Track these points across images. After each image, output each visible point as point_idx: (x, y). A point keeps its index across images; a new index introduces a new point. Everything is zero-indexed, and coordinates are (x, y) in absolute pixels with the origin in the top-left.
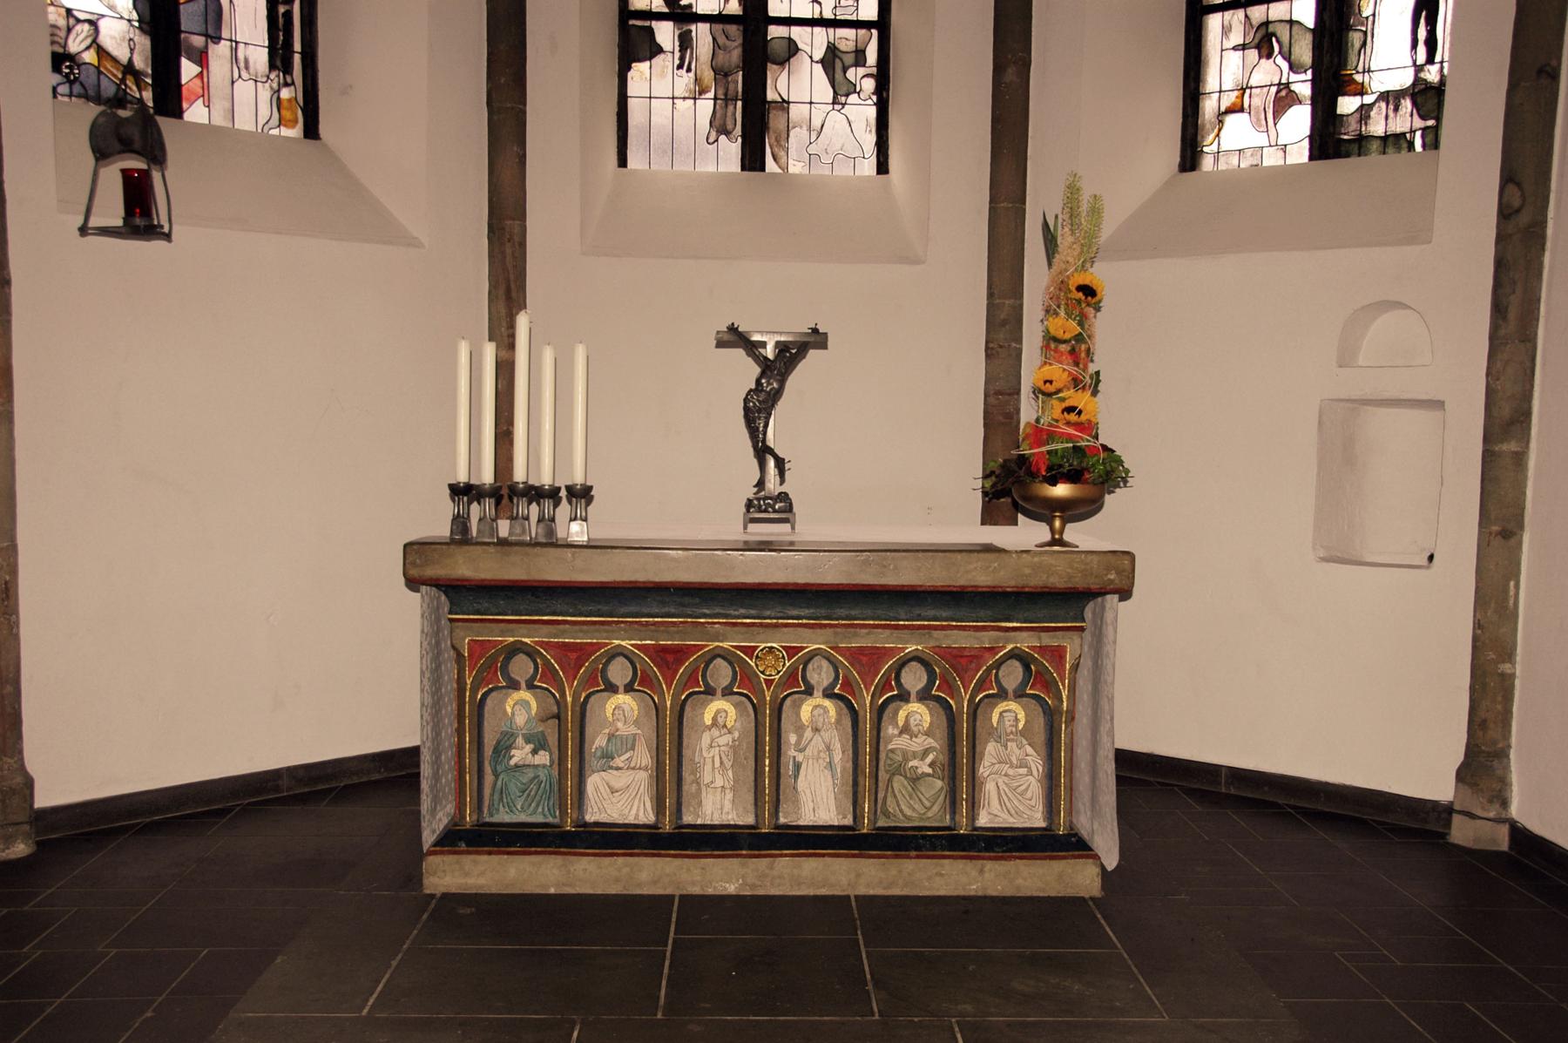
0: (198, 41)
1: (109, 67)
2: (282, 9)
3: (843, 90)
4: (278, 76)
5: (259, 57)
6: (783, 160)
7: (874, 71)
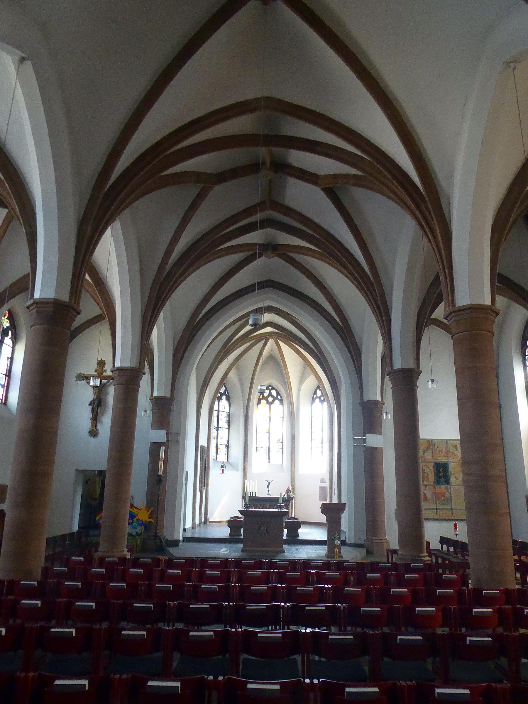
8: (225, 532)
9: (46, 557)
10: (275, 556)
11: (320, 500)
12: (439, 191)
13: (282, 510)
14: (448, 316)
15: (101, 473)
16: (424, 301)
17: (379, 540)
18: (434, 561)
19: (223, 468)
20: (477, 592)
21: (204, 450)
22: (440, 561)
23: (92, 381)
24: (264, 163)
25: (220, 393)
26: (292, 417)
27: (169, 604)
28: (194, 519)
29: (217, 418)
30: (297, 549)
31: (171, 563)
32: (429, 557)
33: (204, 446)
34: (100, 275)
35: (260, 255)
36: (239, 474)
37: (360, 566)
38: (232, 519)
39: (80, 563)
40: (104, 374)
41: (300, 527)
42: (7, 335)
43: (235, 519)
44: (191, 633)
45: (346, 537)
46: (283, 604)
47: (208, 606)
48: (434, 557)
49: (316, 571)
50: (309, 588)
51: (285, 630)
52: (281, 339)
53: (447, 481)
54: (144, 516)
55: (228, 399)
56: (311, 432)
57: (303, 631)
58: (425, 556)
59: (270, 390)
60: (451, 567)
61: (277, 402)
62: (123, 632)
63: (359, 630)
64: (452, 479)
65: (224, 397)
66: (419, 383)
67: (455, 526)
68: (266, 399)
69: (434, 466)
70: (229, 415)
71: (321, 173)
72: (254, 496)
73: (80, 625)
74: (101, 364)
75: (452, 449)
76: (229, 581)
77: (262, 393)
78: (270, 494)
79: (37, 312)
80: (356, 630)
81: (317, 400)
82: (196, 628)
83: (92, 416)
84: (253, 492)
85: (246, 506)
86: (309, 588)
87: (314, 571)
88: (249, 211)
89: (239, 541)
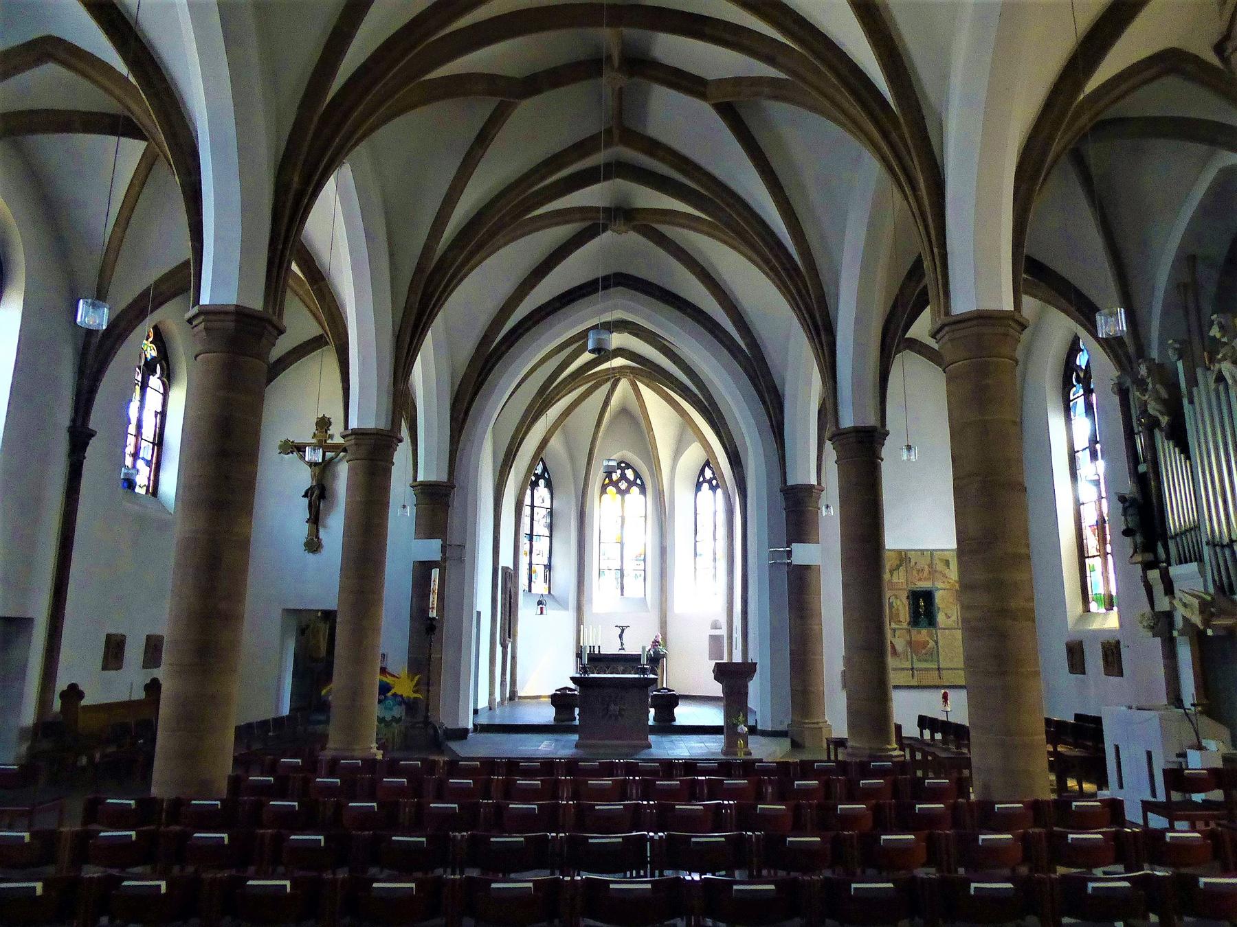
8: (547, 714)
9: (236, 759)
10: (637, 754)
11: (711, 658)
12: (923, 106)
13: (646, 676)
14: (938, 331)
15: (329, 616)
16: (895, 306)
17: (813, 723)
18: (908, 757)
19: (541, 606)
20: (985, 806)
21: (508, 574)
22: (919, 756)
23: (309, 455)
24: (609, 57)
25: (536, 475)
26: (661, 515)
27: (455, 836)
28: (491, 693)
29: (529, 518)
30: (672, 741)
31: (454, 767)
32: (901, 750)
33: (508, 568)
34: (317, 264)
35: (605, 229)
36: (569, 616)
37: (783, 767)
38: (558, 692)
39: (295, 768)
40: (329, 441)
41: (677, 704)
42: (154, 372)
43: (563, 691)
44: (493, 885)
45: (756, 720)
46: (651, 834)
47: (522, 839)
48: (908, 751)
49: (707, 777)
50: (697, 806)
51: (654, 877)
52: (644, 379)
53: (931, 622)
54: (404, 687)
55: (549, 485)
56: (696, 542)
57: (688, 878)
58: (895, 749)
59: (623, 470)
60: (940, 767)
61: (635, 490)
62: (375, 885)
63: (782, 873)
64: (941, 618)
65: (542, 482)
66: (884, 452)
67: (945, 697)
68: (615, 484)
69: (908, 598)
70: (551, 513)
71: (711, 75)
72: (596, 652)
73: (298, 874)
74: (324, 423)
75: (940, 566)
76: (556, 796)
77: (609, 474)
78: (624, 649)
79: (207, 329)
80: (776, 874)
81: (706, 486)
82: (501, 875)
83: (310, 517)
84: (594, 647)
85: (584, 670)
86: (697, 806)
87: (704, 778)
88: (582, 148)
89: (571, 730)
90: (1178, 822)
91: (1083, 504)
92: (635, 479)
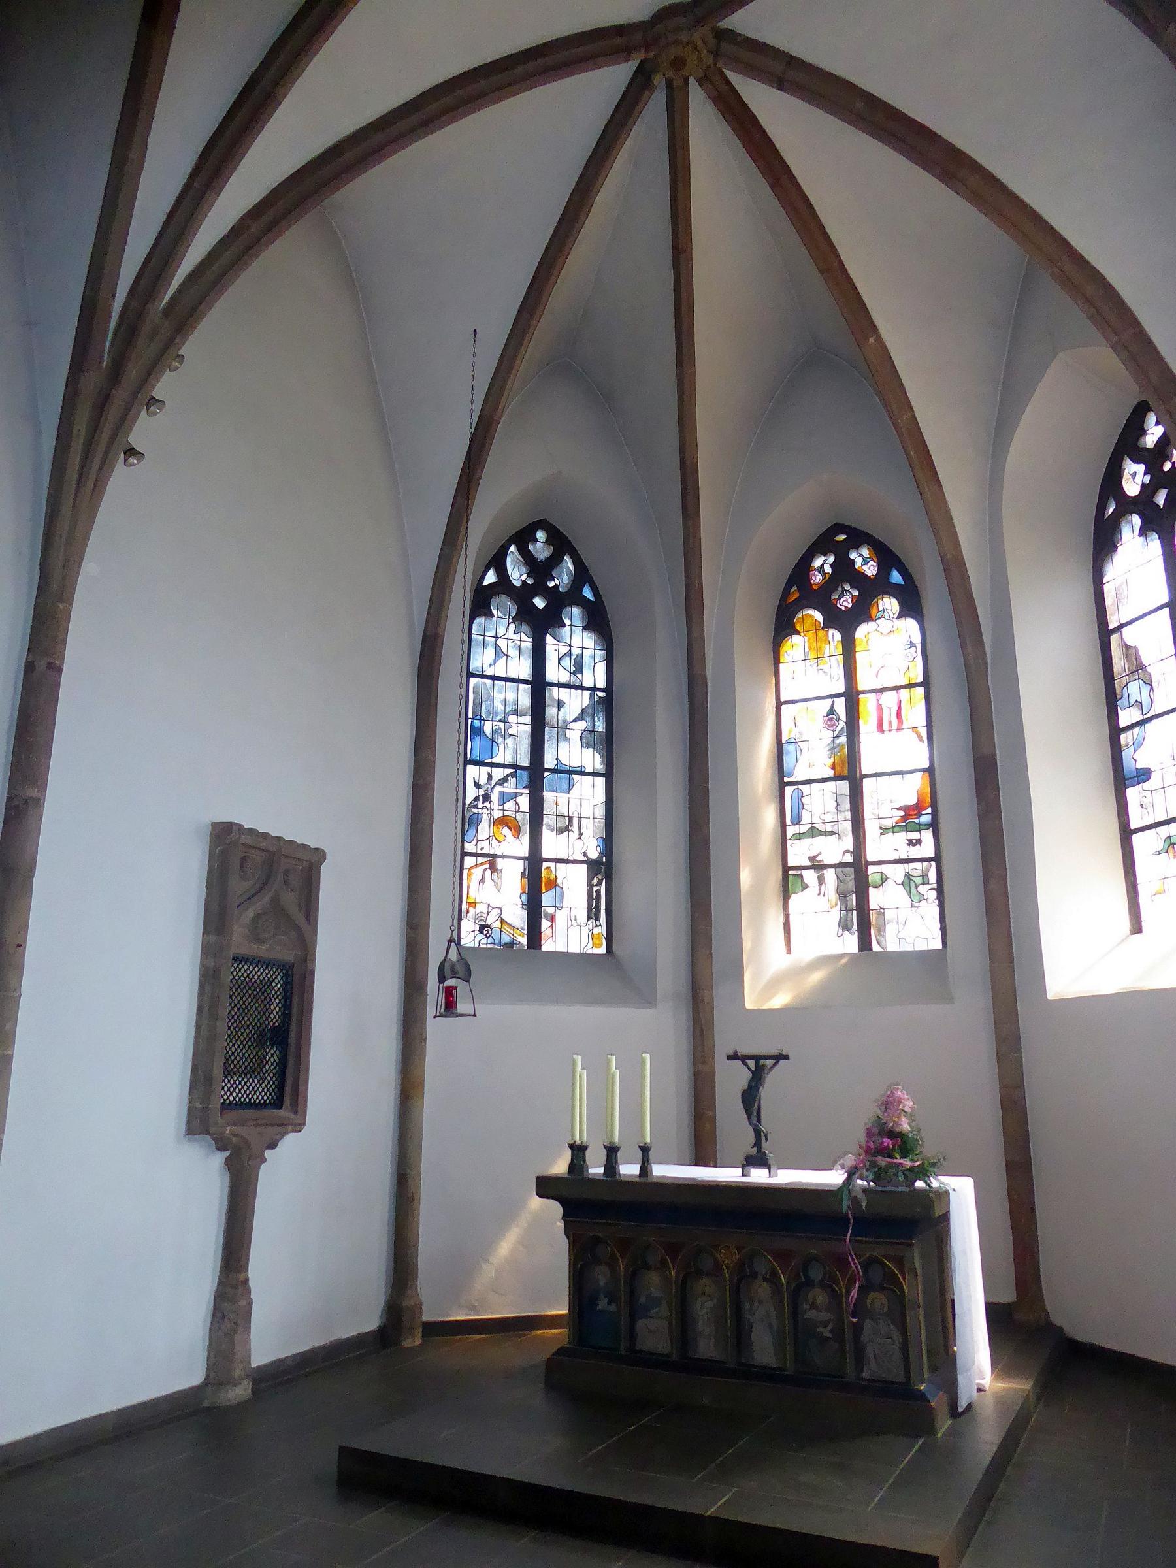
0: (551, 910)
1: (506, 928)
2: (595, 889)
3: (916, 899)
4: (593, 923)
5: (582, 912)
6: (883, 944)
7: (935, 886)
55: (597, 621)
65: (574, 616)
68: (822, 599)
90: (921, 946)
91: (1159, 852)
92: (884, 570)
